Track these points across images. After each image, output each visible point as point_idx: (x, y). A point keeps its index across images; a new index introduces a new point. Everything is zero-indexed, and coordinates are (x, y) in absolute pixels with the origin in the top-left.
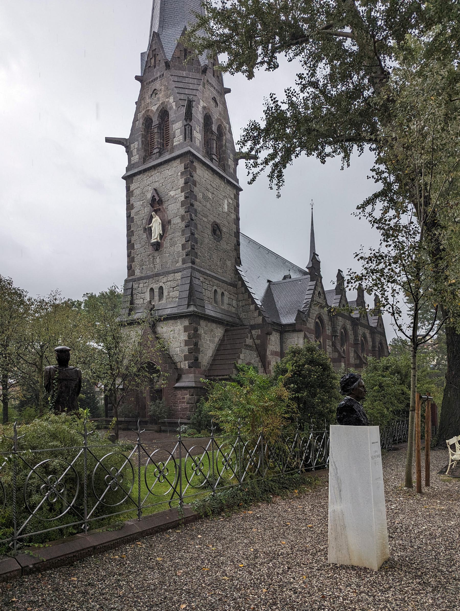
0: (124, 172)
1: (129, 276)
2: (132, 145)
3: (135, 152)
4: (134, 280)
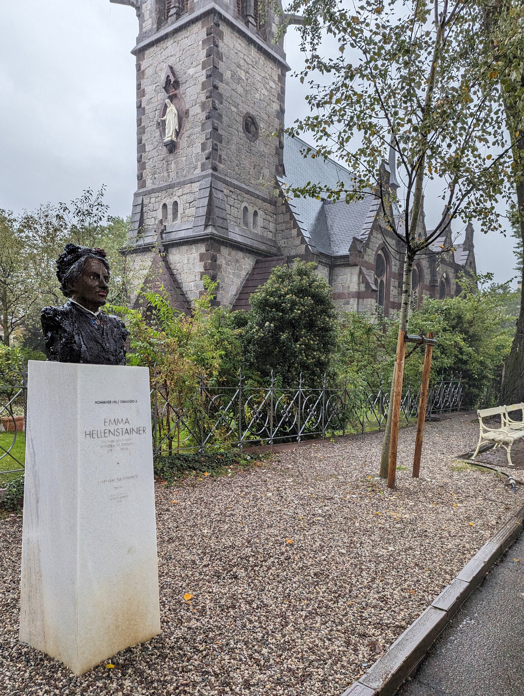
0: (133, 45)
1: (139, 188)
2: (144, 6)
3: (147, 15)
4: (145, 194)
